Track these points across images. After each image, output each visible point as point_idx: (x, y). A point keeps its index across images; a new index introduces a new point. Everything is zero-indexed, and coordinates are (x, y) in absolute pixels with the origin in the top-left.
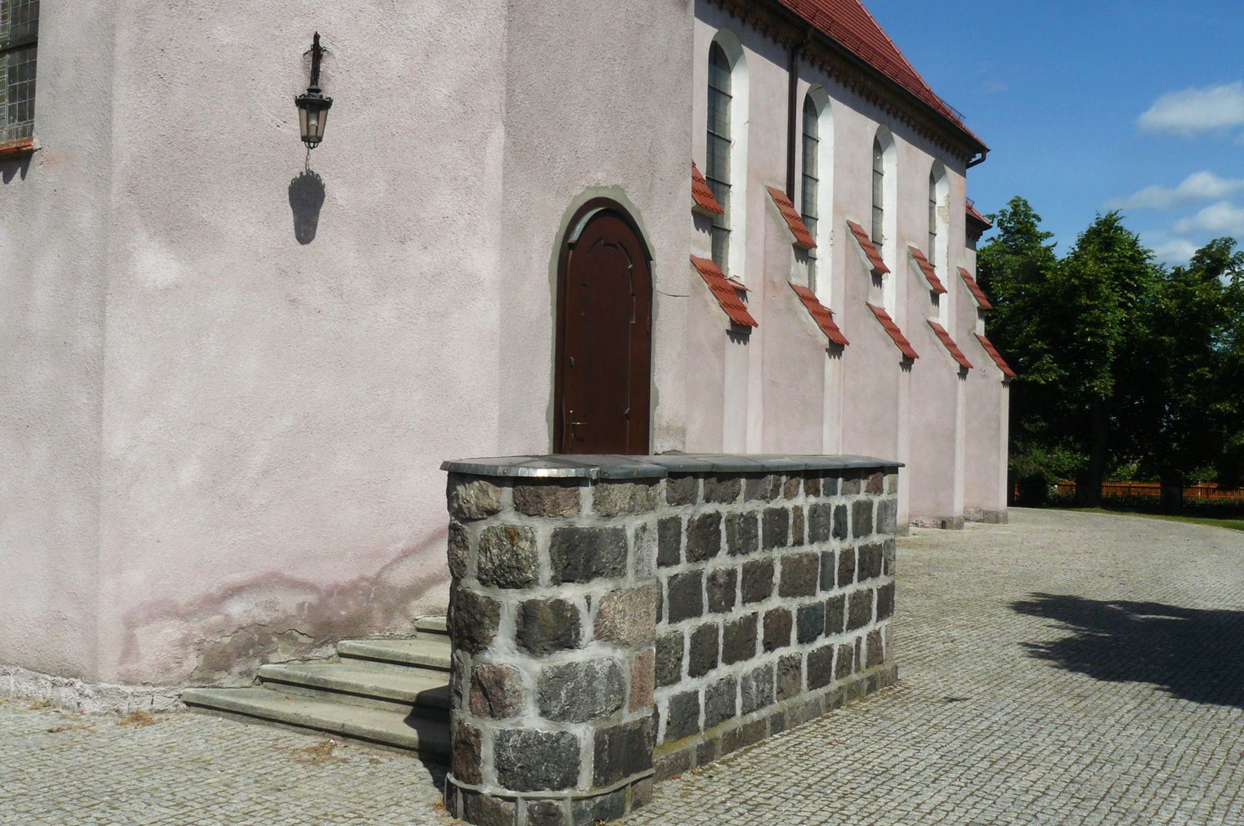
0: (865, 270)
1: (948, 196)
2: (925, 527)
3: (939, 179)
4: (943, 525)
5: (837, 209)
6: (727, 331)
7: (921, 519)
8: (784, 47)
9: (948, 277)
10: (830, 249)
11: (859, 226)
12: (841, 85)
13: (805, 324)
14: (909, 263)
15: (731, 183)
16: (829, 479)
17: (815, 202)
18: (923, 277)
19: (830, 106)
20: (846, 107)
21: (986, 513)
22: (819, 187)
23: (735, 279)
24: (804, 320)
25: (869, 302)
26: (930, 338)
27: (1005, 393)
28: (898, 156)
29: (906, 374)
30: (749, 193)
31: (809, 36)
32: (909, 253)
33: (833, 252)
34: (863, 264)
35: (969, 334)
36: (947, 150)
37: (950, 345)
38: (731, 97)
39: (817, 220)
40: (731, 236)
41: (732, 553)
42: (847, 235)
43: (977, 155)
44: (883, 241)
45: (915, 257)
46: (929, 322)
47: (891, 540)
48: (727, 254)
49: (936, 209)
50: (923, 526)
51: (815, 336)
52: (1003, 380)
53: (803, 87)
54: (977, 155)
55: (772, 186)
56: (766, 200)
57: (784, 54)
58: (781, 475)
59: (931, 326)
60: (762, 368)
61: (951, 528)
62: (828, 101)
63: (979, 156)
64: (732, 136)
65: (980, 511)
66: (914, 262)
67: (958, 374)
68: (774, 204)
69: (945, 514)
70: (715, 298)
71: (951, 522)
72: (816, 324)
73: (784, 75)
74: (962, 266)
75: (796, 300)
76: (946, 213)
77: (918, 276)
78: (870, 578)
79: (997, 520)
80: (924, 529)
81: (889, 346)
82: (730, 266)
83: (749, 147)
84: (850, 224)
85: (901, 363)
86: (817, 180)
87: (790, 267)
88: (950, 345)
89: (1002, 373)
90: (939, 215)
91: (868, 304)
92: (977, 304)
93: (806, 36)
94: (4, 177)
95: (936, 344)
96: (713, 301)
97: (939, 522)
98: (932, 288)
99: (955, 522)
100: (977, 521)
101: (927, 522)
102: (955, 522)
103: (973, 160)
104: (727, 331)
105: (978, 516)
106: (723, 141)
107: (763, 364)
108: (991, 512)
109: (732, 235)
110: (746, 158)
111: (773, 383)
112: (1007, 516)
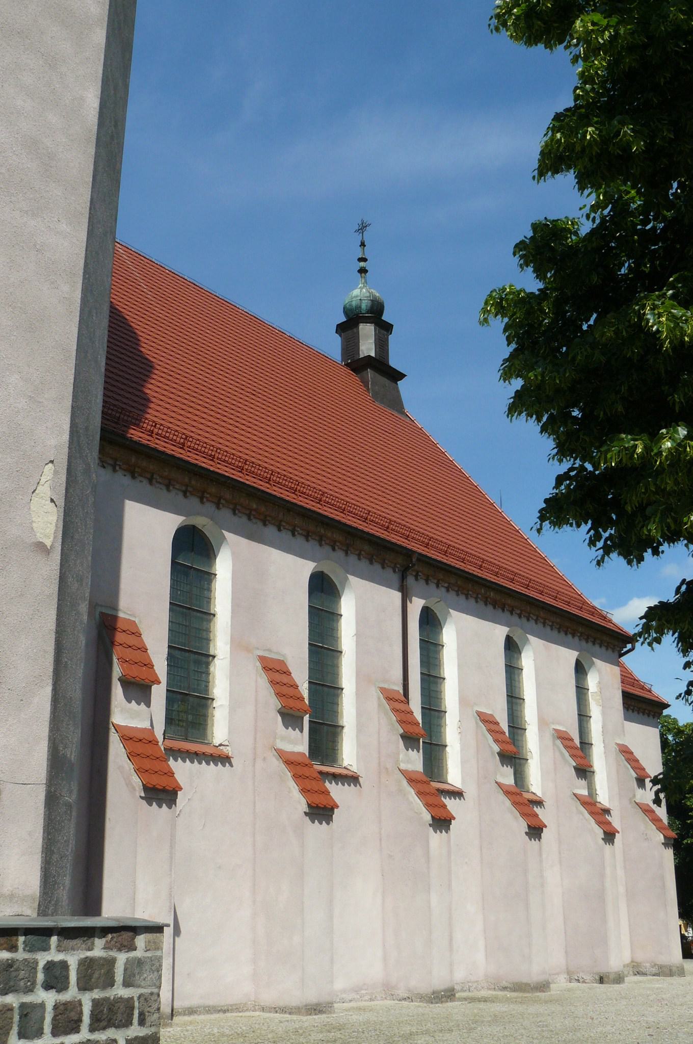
0: (493, 753)
1: (599, 683)
2: (586, 983)
3: (589, 669)
4: (601, 980)
5: (463, 701)
6: (305, 813)
7: (581, 975)
8: (394, 571)
9: (605, 753)
10: (458, 737)
11: (492, 715)
12: (463, 597)
13: (412, 803)
14: (554, 744)
15: (343, 687)
16: (150, 936)
17: (443, 697)
18: (567, 754)
19: (451, 616)
20: (468, 617)
21: (661, 967)
22: (446, 684)
23: (349, 767)
24: (411, 799)
25: (498, 781)
26: (577, 808)
27: (669, 855)
28: (534, 654)
29: (534, 843)
30: (359, 694)
31: (414, 560)
32: (553, 734)
33: (461, 740)
34: (490, 747)
35: (631, 802)
36: (594, 644)
37: (314, 814)
38: (341, 615)
39: (446, 712)
40: (344, 731)
41: (42, 1006)
42: (477, 723)
43: (627, 645)
44: (527, 727)
45: (559, 738)
46: (574, 794)
47: (152, 994)
48: (342, 746)
49: (589, 693)
50: (584, 982)
51: (421, 813)
52: (663, 841)
53: (416, 605)
54: (627, 645)
55: (386, 686)
56: (379, 698)
57: (395, 578)
58: (50, 936)
59: (577, 798)
60: (381, 844)
61: (607, 983)
62: (449, 612)
63: (629, 646)
64: (343, 647)
65: (655, 965)
66: (558, 742)
67: (603, 839)
68: (384, 702)
69: (603, 969)
70: (295, 785)
71: (608, 977)
72: (421, 803)
73: (397, 596)
74: (621, 742)
75: (405, 782)
76: (598, 697)
77: (561, 753)
78: (113, 1028)
79: (671, 974)
80: (584, 984)
81: (516, 818)
82: (344, 757)
83: (357, 654)
84: (479, 714)
85: (526, 833)
86: (444, 679)
87: (399, 754)
88: (314, 814)
89: (662, 835)
90: (592, 699)
91: (496, 782)
92: (635, 775)
93: (412, 560)
94: (666, 708)
95: (582, 813)
96: (294, 787)
97: (598, 978)
98: (575, 764)
99: (612, 977)
100: (654, 975)
101: (587, 977)
102: (612, 977)
103: (625, 650)
104: (305, 813)
105: (654, 970)
106: (332, 652)
107: (381, 840)
108: (665, 966)
109: (345, 730)
110: (354, 665)
111: (390, 856)
112: (683, 969)
